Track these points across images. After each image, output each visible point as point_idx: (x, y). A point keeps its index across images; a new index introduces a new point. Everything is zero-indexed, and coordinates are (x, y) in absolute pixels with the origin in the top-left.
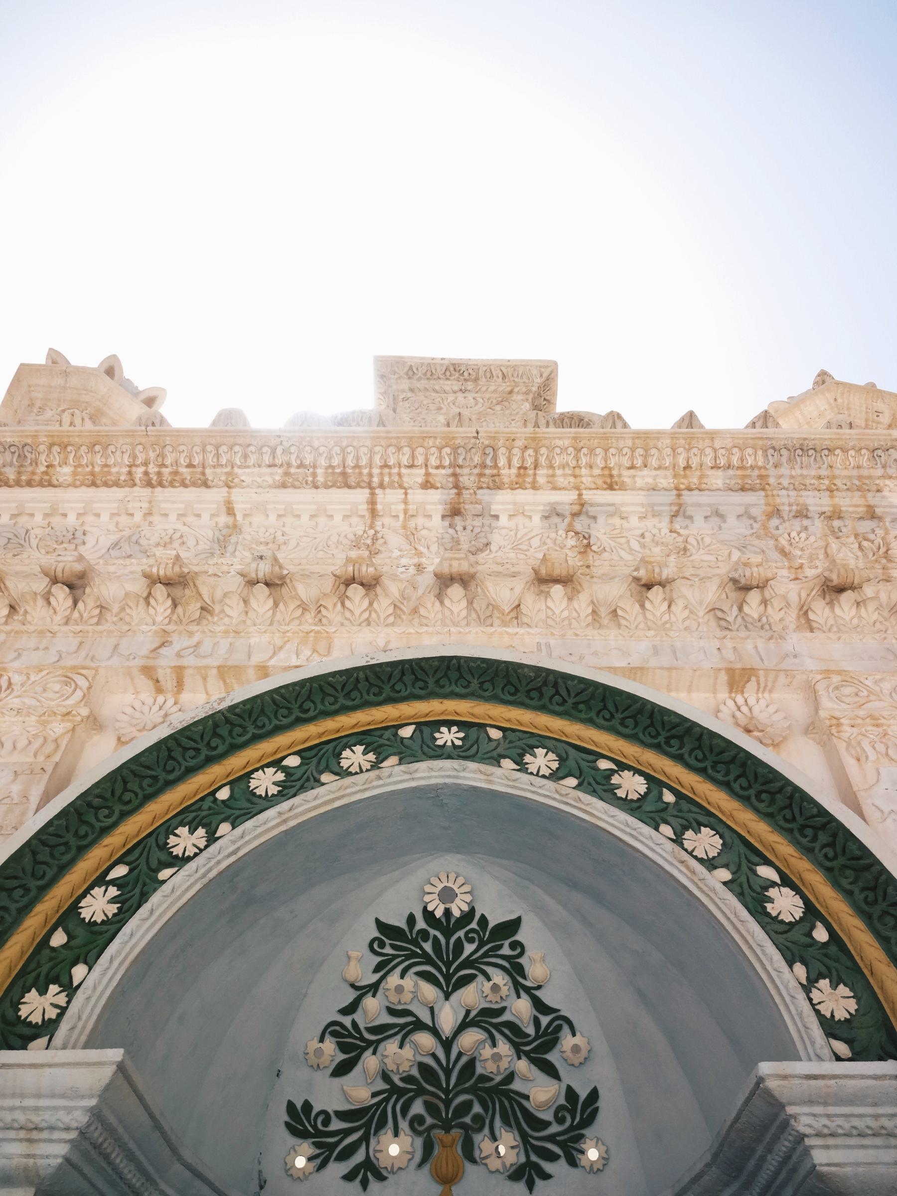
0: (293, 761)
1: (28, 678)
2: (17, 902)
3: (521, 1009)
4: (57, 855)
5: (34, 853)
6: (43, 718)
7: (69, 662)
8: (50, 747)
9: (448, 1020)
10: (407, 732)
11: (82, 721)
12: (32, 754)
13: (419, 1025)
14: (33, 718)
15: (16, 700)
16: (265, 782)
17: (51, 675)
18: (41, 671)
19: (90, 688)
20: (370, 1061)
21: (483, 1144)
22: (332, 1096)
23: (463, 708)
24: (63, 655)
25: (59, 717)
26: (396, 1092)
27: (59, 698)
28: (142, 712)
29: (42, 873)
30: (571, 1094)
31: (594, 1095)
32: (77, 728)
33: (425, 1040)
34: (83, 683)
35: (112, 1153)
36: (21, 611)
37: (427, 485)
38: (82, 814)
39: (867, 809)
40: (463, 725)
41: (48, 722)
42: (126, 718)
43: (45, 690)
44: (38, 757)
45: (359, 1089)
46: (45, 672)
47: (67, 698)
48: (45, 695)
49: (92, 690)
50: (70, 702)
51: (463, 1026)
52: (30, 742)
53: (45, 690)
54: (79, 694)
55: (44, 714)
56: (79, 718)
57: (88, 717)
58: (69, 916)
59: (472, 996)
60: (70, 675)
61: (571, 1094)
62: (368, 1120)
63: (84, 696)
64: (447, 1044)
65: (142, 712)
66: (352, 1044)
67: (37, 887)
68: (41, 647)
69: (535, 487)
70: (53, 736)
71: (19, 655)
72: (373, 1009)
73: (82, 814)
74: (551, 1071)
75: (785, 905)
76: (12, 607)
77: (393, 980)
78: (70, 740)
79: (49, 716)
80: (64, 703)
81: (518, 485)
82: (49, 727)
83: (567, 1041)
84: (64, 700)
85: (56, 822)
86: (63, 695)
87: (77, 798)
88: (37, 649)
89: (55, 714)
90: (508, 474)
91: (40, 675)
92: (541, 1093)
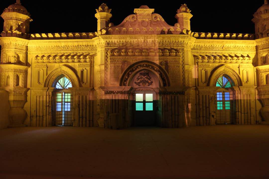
0: (135, 67)
3: (149, 77)
9: (144, 78)
10: (142, 65)
13: (142, 78)
16: (127, 77)
20: (139, 80)
21: (146, 84)
22: (137, 81)
23: (146, 63)
26: (141, 82)
30: (151, 82)
31: (153, 82)
33: (143, 79)
35: (224, 107)
37: (142, 38)
39: (159, 81)
40: (146, 64)
45: (139, 81)
51: (145, 78)
58: (125, 78)
59: (145, 77)
61: (151, 82)
62: (139, 83)
64: (144, 79)
66: (138, 79)
69: (151, 39)
72: (139, 77)
74: (150, 80)
75: (156, 69)
77: (141, 76)
81: (150, 38)
83: (151, 79)
90: (149, 38)
92: (150, 82)
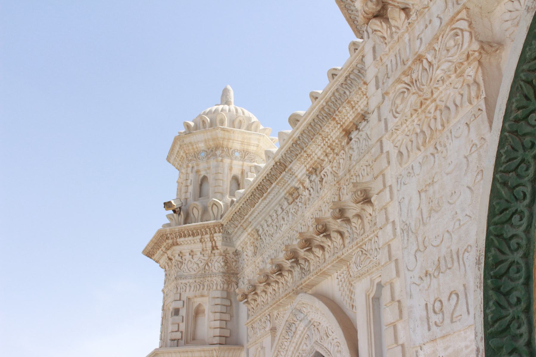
1: (435, 50)
2: (520, 226)
4: (524, 174)
5: (505, 184)
6: (458, 72)
7: (446, 19)
8: (474, 88)
11: (480, 53)
12: (467, 103)
14: (453, 76)
15: (439, 72)
17: (444, 37)
18: (438, 39)
19: (470, 25)
24: (442, 16)
25: (466, 63)
27: (458, 48)
28: (517, 10)
29: (522, 194)
32: (482, 61)
34: (464, 25)
36: (411, 7)
38: (517, 131)
41: (463, 72)
42: (509, 24)
43: (448, 50)
44: (473, 103)
46: (440, 38)
47: (462, 44)
48: (450, 54)
49: (474, 25)
50: (466, 45)
52: (462, 95)
53: (448, 50)
54: (467, 35)
55: (456, 69)
56: (477, 54)
57: (482, 48)
60: (454, 26)
63: (471, 33)
65: (517, 10)
67: (527, 206)
68: (428, 23)
70: (470, 80)
71: (421, 39)
73: (517, 131)
76: (404, 9)
78: (483, 73)
79: (460, 67)
80: (463, 50)
82: (465, 75)
84: (462, 47)
85: (502, 151)
86: (459, 44)
87: (504, 122)
88: (426, 27)
89: (462, 63)
91: (439, 42)
